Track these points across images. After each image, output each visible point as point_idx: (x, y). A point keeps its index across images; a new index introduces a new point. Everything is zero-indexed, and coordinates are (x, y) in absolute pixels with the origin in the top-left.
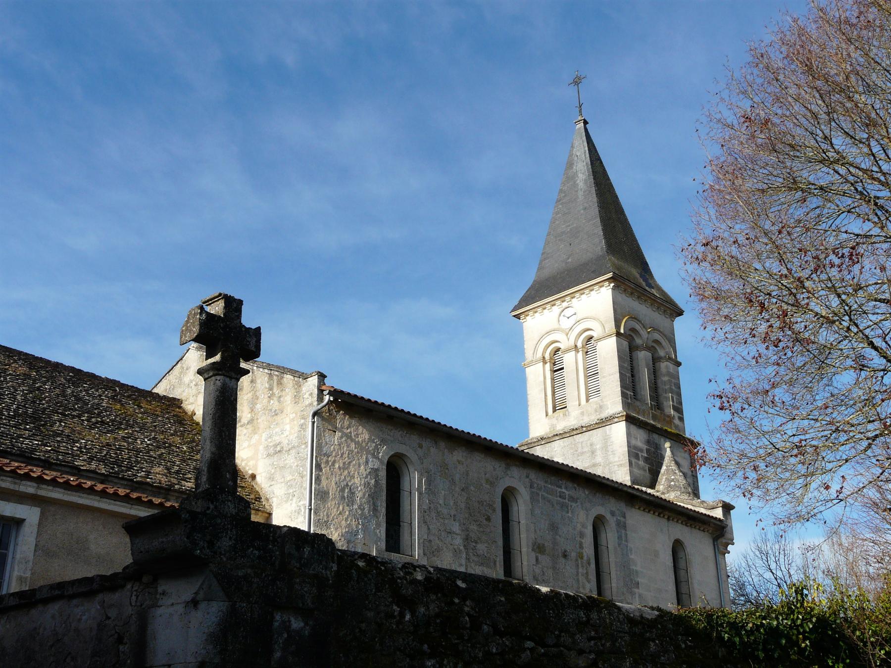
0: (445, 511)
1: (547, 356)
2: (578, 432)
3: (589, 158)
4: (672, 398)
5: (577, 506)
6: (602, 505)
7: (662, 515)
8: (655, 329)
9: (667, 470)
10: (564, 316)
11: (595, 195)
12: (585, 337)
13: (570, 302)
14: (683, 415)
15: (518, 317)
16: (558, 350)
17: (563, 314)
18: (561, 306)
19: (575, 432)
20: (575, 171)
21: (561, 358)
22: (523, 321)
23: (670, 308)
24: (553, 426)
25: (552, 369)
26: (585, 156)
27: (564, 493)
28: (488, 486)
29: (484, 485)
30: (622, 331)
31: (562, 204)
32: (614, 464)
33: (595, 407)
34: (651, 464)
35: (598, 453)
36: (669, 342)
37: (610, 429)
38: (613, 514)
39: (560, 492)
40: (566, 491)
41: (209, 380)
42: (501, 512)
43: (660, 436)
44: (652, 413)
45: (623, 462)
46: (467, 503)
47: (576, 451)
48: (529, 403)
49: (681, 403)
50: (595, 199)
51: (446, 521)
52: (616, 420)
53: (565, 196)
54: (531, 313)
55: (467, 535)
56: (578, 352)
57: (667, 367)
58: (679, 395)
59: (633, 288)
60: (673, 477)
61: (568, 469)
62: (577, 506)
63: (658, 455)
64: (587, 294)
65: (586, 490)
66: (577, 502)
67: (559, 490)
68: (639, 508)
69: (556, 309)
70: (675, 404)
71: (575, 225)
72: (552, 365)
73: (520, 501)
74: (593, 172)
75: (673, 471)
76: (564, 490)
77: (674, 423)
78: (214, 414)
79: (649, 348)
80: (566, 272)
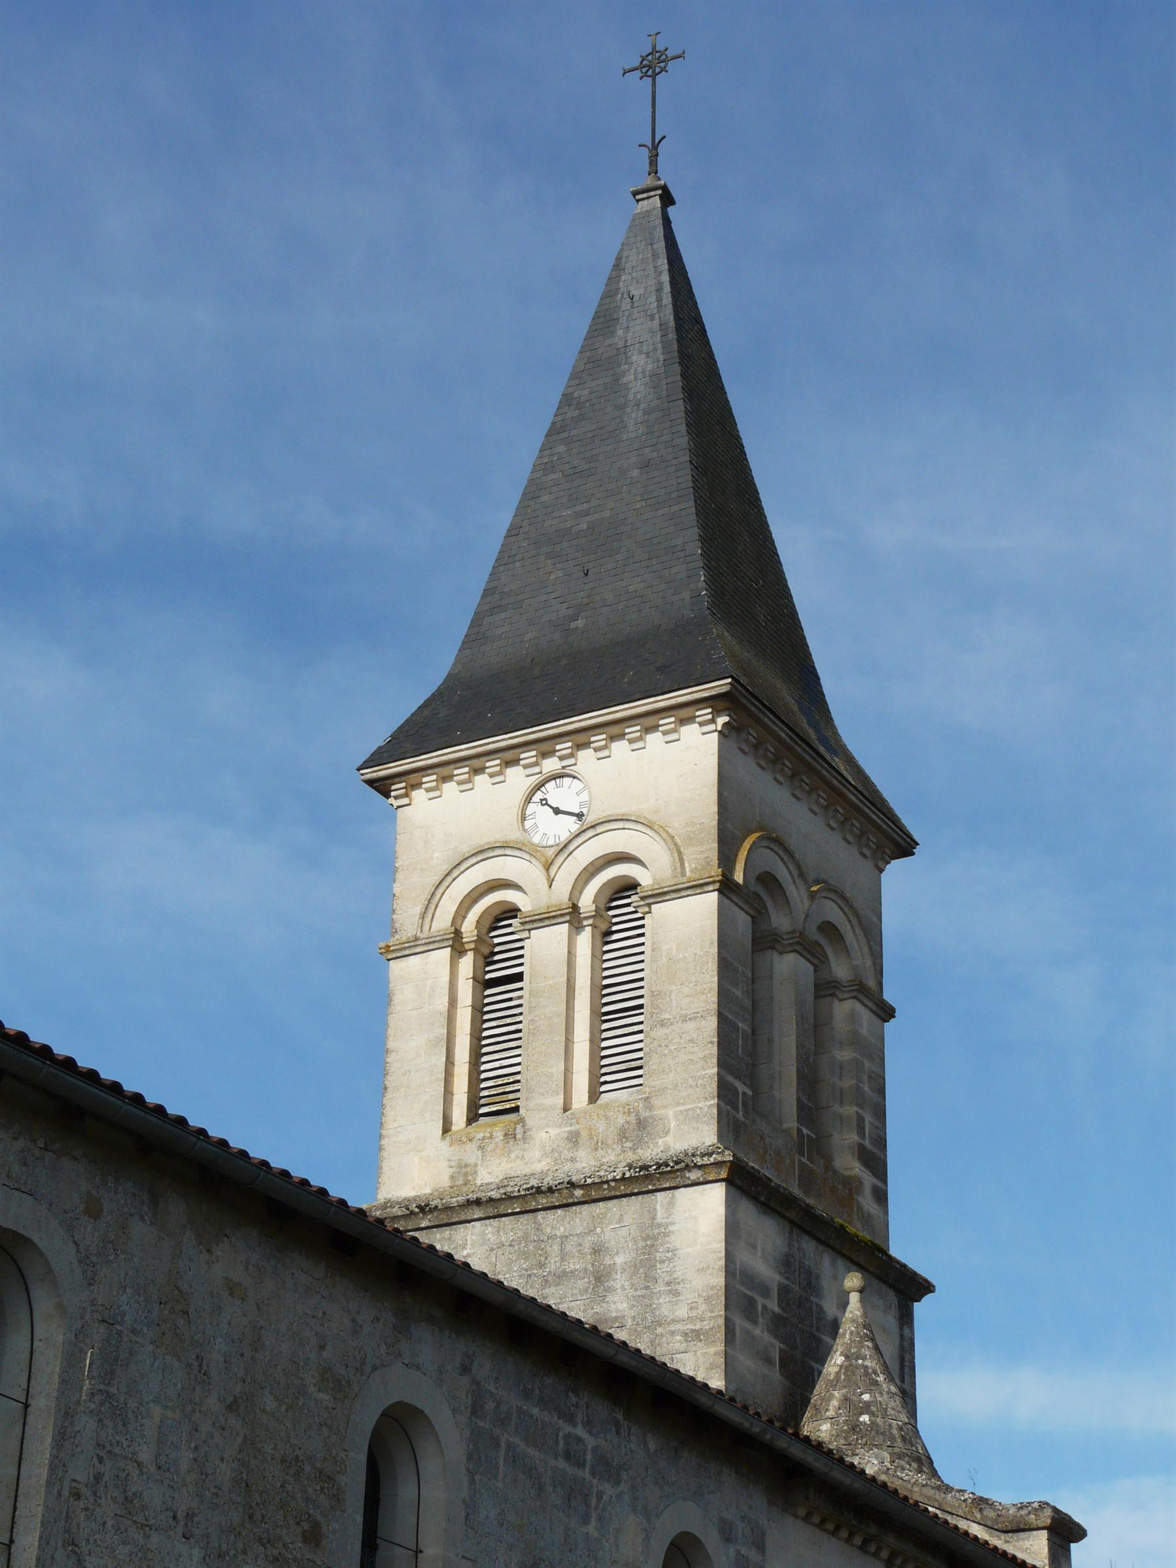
1: (469, 928)
2: (555, 1200)
3: (669, 310)
5: (620, 1496)
7: (872, 1548)
8: (835, 892)
9: (848, 1368)
10: (544, 802)
12: (610, 881)
13: (571, 761)
14: (885, 1183)
15: (382, 786)
16: (512, 912)
17: (538, 796)
18: (536, 769)
19: (543, 1201)
20: (621, 344)
21: (518, 945)
22: (396, 803)
24: (464, 1171)
25: (480, 974)
26: (659, 300)
27: (580, 1440)
28: (325, 1397)
29: (312, 1389)
30: (739, 877)
32: (672, 1327)
33: (621, 1120)
35: (617, 1284)
36: (868, 941)
37: (671, 1203)
38: (727, 1533)
39: (568, 1437)
42: (361, 1504)
43: (821, 1248)
45: (706, 1325)
47: (541, 1265)
49: (881, 1143)
50: (683, 441)
51: (155, 1539)
52: (694, 1175)
54: (429, 780)
57: (852, 1017)
58: (880, 1114)
60: (866, 1397)
61: (609, 1351)
62: (620, 1496)
64: (631, 741)
65: (649, 1437)
66: (617, 1482)
67: (567, 1428)
68: (807, 1519)
69: (518, 779)
70: (867, 1143)
71: (607, 514)
72: (481, 962)
73: (430, 1466)
74: (681, 353)
75: (867, 1374)
76: (580, 1431)
77: (860, 1208)
80: (564, 662)
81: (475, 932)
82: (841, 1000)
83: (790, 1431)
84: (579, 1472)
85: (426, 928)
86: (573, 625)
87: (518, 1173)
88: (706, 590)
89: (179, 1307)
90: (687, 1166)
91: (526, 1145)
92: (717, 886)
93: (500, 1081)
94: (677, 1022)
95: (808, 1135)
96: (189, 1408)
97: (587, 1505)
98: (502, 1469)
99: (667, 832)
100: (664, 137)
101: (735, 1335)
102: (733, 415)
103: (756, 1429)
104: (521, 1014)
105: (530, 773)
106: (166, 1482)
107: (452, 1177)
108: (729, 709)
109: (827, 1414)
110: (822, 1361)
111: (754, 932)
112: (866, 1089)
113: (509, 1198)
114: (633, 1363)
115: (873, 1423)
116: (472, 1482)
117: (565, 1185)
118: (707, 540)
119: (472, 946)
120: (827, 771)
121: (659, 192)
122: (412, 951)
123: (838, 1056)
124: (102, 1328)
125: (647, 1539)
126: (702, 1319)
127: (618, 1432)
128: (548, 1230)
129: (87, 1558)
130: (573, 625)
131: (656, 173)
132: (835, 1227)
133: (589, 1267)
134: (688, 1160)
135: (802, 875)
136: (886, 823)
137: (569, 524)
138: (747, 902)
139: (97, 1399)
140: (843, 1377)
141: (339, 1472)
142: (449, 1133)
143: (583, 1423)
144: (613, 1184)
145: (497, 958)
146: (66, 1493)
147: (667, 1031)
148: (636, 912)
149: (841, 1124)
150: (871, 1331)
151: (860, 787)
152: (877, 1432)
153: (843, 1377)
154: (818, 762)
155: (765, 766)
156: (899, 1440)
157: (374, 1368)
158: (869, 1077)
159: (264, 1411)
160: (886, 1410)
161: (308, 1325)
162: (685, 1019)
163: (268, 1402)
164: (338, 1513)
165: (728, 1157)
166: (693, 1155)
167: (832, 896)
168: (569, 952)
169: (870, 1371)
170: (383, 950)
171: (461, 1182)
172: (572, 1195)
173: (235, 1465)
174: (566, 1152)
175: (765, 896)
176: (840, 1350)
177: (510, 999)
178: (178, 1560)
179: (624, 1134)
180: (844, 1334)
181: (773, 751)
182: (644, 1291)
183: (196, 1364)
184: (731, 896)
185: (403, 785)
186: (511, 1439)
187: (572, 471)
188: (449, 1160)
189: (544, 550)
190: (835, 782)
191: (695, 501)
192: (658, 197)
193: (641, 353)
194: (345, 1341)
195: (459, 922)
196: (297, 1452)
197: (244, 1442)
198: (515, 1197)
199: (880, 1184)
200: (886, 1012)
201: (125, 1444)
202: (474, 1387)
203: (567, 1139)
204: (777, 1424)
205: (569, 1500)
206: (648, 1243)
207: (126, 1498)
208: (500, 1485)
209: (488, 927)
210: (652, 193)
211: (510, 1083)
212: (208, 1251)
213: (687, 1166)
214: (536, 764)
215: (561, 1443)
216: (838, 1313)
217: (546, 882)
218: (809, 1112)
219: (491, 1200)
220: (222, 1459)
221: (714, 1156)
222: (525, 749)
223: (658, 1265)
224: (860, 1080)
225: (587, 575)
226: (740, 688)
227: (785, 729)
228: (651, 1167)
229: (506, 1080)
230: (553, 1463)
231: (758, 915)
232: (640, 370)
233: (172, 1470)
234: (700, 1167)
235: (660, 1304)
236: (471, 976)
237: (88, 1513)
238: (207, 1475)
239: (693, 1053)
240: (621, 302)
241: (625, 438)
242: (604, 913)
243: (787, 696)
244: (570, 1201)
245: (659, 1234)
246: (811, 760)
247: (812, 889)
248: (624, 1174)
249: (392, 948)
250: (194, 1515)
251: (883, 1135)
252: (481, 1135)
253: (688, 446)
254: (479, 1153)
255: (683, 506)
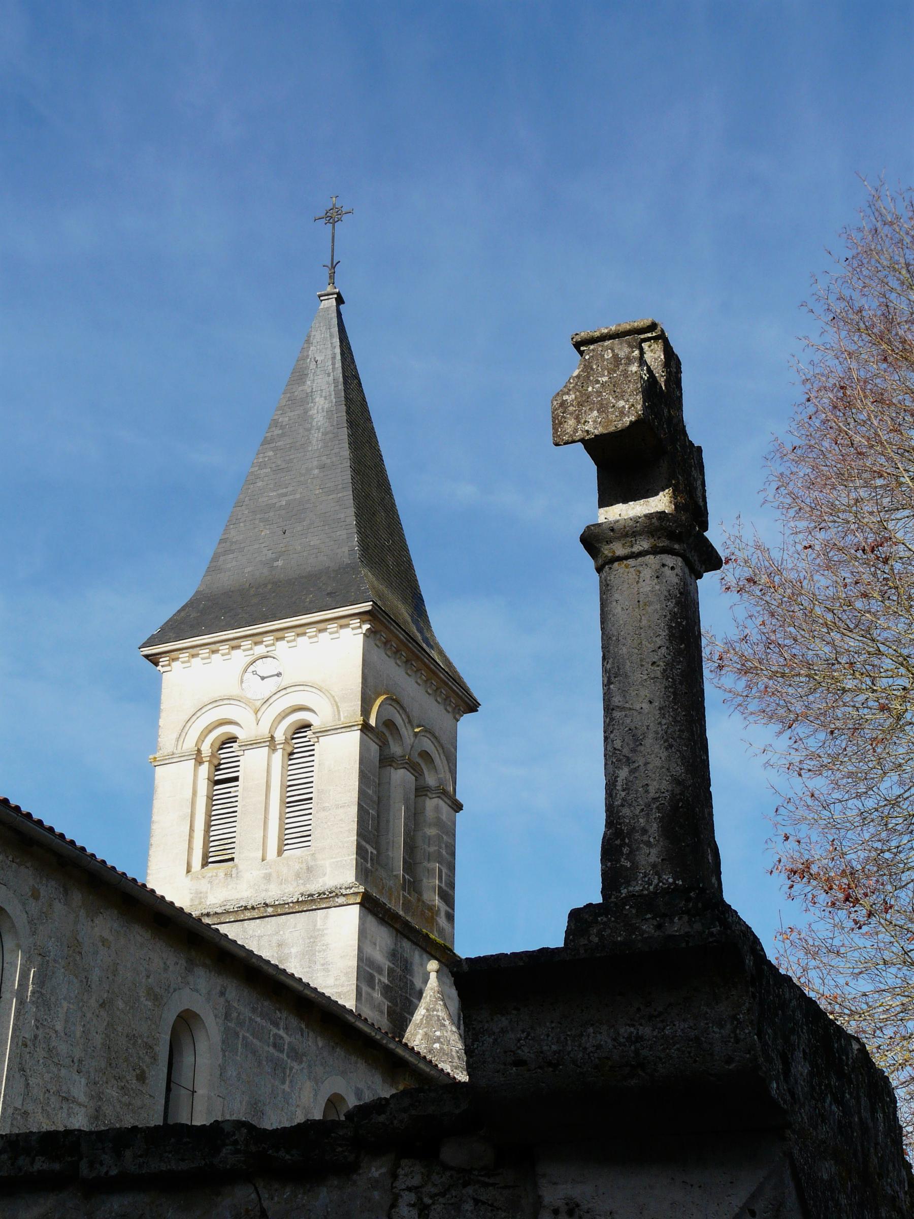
0: (63, 1048)
1: (206, 749)
2: (255, 914)
3: (340, 370)
4: (440, 871)
6: (343, 1073)
8: (429, 731)
9: (428, 1017)
11: (347, 445)
13: (272, 648)
14: (453, 909)
15: (154, 659)
16: (233, 739)
17: (252, 668)
18: (251, 652)
19: (248, 914)
20: (309, 390)
21: (236, 760)
22: (162, 670)
23: (457, 694)
25: (212, 775)
26: (333, 364)
27: (281, 1038)
29: (142, 999)
30: (372, 722)
31: (275, 450)
33: (297, 867)
34: (392, 1000)
36: (448, 763)
37: (326, 917)
39: (275, 1035)
40: (285, 1036)
41: (631, 562)
43: (414, 947)
44: (404, 896)
45: (345, 989)
46: (107, 1036)
48: (154, 841)
49: (452, 885)
50: (346, 453)
51: (63, 1072)
52: (341, 900)
53: (283, 435)
54: (184, 656)
55: (98, 1110)
56: (274, 750)
57: (437, 809)
58: (452, 868)
59: (401, 641)
60: (438, 1033)
63: (406, 983)
64: (310, 637)
65: (319, 1038)
66: (301, 1062)
67: (275, 1031)
69: (240, 657)
70: (443, 885)
71: (298, 496)
72: (213, 769)
73: (202, 1046)
74: (346, 398)
75: (439, 1020)
76: (281, 1033)
78: (670, 665)
79: (414, 768)
80: (269, 587)
81: (210, 751)
82: (430, 798)
83: (397, 1039)
84: (281, 1055)
85: (179, 747)
86: (275, 564)
87: (233, 898)
88: (358, 546)
89: (77, 950)
90: (337, 894)
91: (239, 881)
92: (360, 727)
93: (222, 842)
94: (333, 808)
95: (409, 880)
96: (81, 1004)
97: (285, 1074)
98: (240, 1050)
99: (330, 694)
100: (339, 262)
101: (362, 995)
102: (376, 436)
103: (378, 1037)
104: (237, 801)
105: (248, 654)
106: (69, 1042)
107: (192, 900)
108: (370, 620)
109: (415, 1043)
110: (412, 1014)
111: (380, 756)
112: (444, 853)
113: (228, 912)
114: (313, 995)
115: (441, 1049)
116: (224, 1056)
117: (262, 905)
118: (360, 515)
119: (208, 759)
120: (428, 659)
121: (336, 296)
122: (170, 761)
123: (428, 832)
124: (39, 958)
125: (316, 1095)
126: (342, 986)
127: (302, 1035)
128: (251, 932)
129: (30, 1078)
130: (275, 564)
131: (333, 284)
132: (423, 935)
133: (275, 954)
134: (337, 891)
135: (410, 722)
136: (462, 692)
137: (274, 501)
138: (377, 737)
139: (36, 995)
140: (425, 1022)
141: (155, 1045)
142: (190, 873)
143: (283, 1029)
144: (291, 905)
145: (222, 767)
146: (20, 1044)
147: (327, 814)
148: (310, 741)
149: (428, 873)
150: (442, 995)
151: (447, 670)
152: (444, 1053)
153: (425, 1022)
154: (422, 654)
155: (400, 664)
156: (456, 1058)
157: (175, 990)
158: (446, 846)
159: (118, 1009)
160: (449, 1041)
161: (141, 964)
162: (337, 807)
163: (120, 1004)
164: (155, 1066)
165: (362, 889)
166: (341, 888)
167: (428, 735)
168: (268, 764)
169: (441, 1018)
170: (152, 760)
171: (196, 903)
172: (266, 911)
173: (104, 1035)
174: (263, 885)
175: (387, 734)
176: (424, 1005)
177: (230, 792)
178: (74, 1084)
179: (299, 875)
180: (426, 997)
181: (395, 646)
182: (308, 969)
183: (85, 980)
184: (367, 733)
185: (168, 658)
186: (245, 1034)
187: (277, 468)
188: (190, 889)
189: (258, 516)
190: (432, 666)
191: (353, 492)
192: (334, 299)
193: (321, 396)
194: (160, 974)
195: (200, 744)
196: (134, 1032)
197: (108, 1024)
198: (231, 912)
199: (450, 911)
200: (457, 807)
201: (49, 1020)
202: (227, 1004)
203: (264, 877)
204: (390, 1035)
205: (275, 1070)
206: (312, 940)
207: (49, 1049)
208: (238, 1058)
209: (218, 747)
210: (331, 297)
211: (229, 843)
212: (92, 920)
213: (337, 894)
214: (251, 649)
215: (272, 1038)
216: (423, 986)
217: (255, 721)
218: (409, 866)
219: (216, 913)
220: (97, 1033)
221: (353, 889)
222: (244, 640)
223: (317, 953)
224: (440, 847)
225: (284, 533)
226: (377, 608)
227: (403, 633)
228: (314, 895)
229: (226, 841)
230: (266, 1048)
231: (383, 745)
232: (320, 408)
233: (72, 1036)
234: (344, 895)
235: (317, 977)
236: (207, 777)
237: (31, 1055)
238: (89, 1040)
239: (342, 827)
240: (310, 364)
241: (310, 449)
242: (290, 741)
243: (404, 612)
244: (265, 915)
245: (318, 935)
246: (418, 652)
247: (415, 730)
248: (298, 899)
249: (157, 759)
250: (82, 1061)
251: (452, 880)
252: (210, 875)
253: (349, 457)
254: (209, 885)
255: (345, 494)
